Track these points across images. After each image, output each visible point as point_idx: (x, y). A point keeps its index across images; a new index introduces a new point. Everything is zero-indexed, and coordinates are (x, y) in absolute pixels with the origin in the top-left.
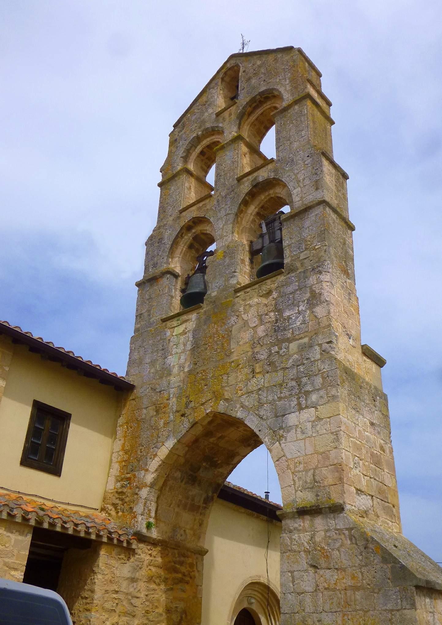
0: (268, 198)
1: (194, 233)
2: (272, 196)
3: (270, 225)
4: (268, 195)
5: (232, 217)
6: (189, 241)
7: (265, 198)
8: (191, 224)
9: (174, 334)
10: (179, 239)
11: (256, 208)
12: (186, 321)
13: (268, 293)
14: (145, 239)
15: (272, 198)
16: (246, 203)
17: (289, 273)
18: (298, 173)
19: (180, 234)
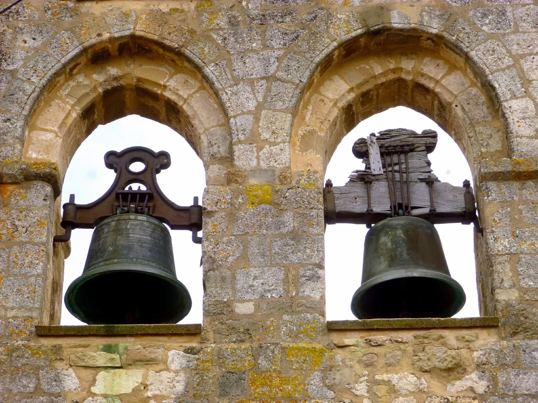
0: (391, 77)
1: (116, 79)
2: (403, 76)
3: (395, 159)
4: (393, 71)
5: (289, 94)
6: (93, 95)
7: (383, 74)
8: (113, 48)
9: (94, 389)
10: (62, 79)
11: (351, 90)
12: (147, 362)
13: (449, 370)
14: (361, 137)
15: (400, 80)
16: (328, 67)
17: (515, 334)
18: (523, 56)
19: (71, 66)
